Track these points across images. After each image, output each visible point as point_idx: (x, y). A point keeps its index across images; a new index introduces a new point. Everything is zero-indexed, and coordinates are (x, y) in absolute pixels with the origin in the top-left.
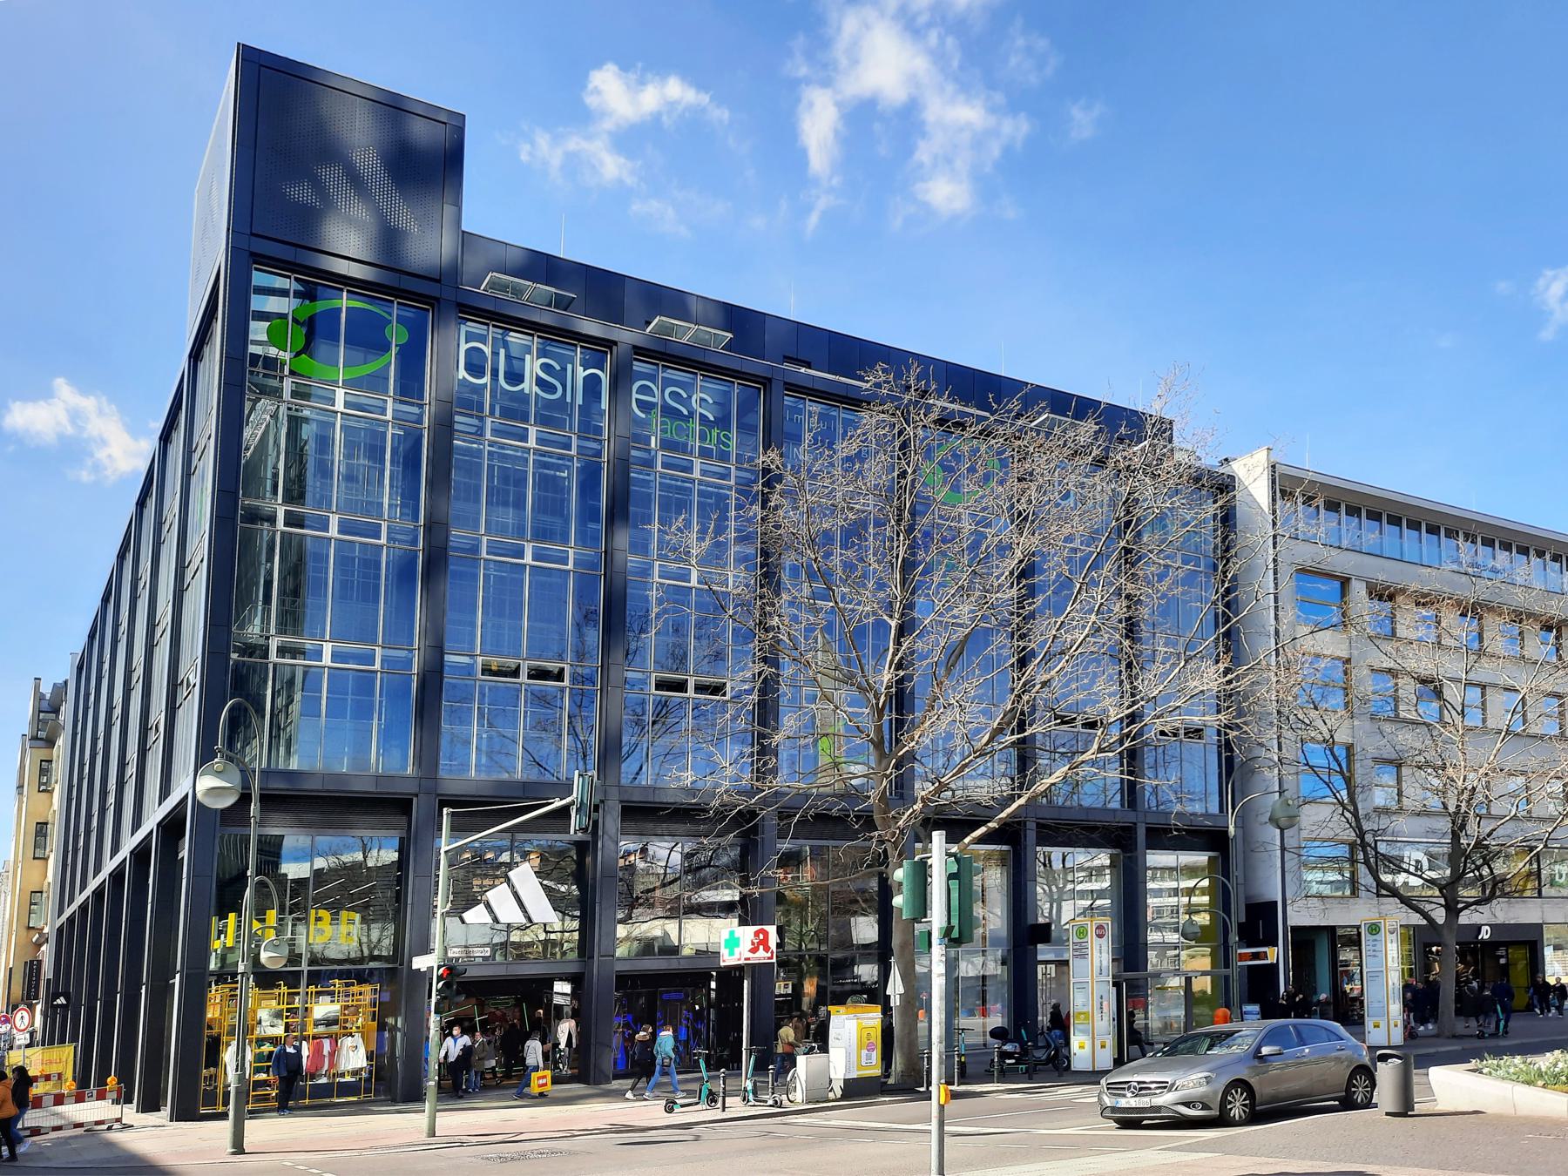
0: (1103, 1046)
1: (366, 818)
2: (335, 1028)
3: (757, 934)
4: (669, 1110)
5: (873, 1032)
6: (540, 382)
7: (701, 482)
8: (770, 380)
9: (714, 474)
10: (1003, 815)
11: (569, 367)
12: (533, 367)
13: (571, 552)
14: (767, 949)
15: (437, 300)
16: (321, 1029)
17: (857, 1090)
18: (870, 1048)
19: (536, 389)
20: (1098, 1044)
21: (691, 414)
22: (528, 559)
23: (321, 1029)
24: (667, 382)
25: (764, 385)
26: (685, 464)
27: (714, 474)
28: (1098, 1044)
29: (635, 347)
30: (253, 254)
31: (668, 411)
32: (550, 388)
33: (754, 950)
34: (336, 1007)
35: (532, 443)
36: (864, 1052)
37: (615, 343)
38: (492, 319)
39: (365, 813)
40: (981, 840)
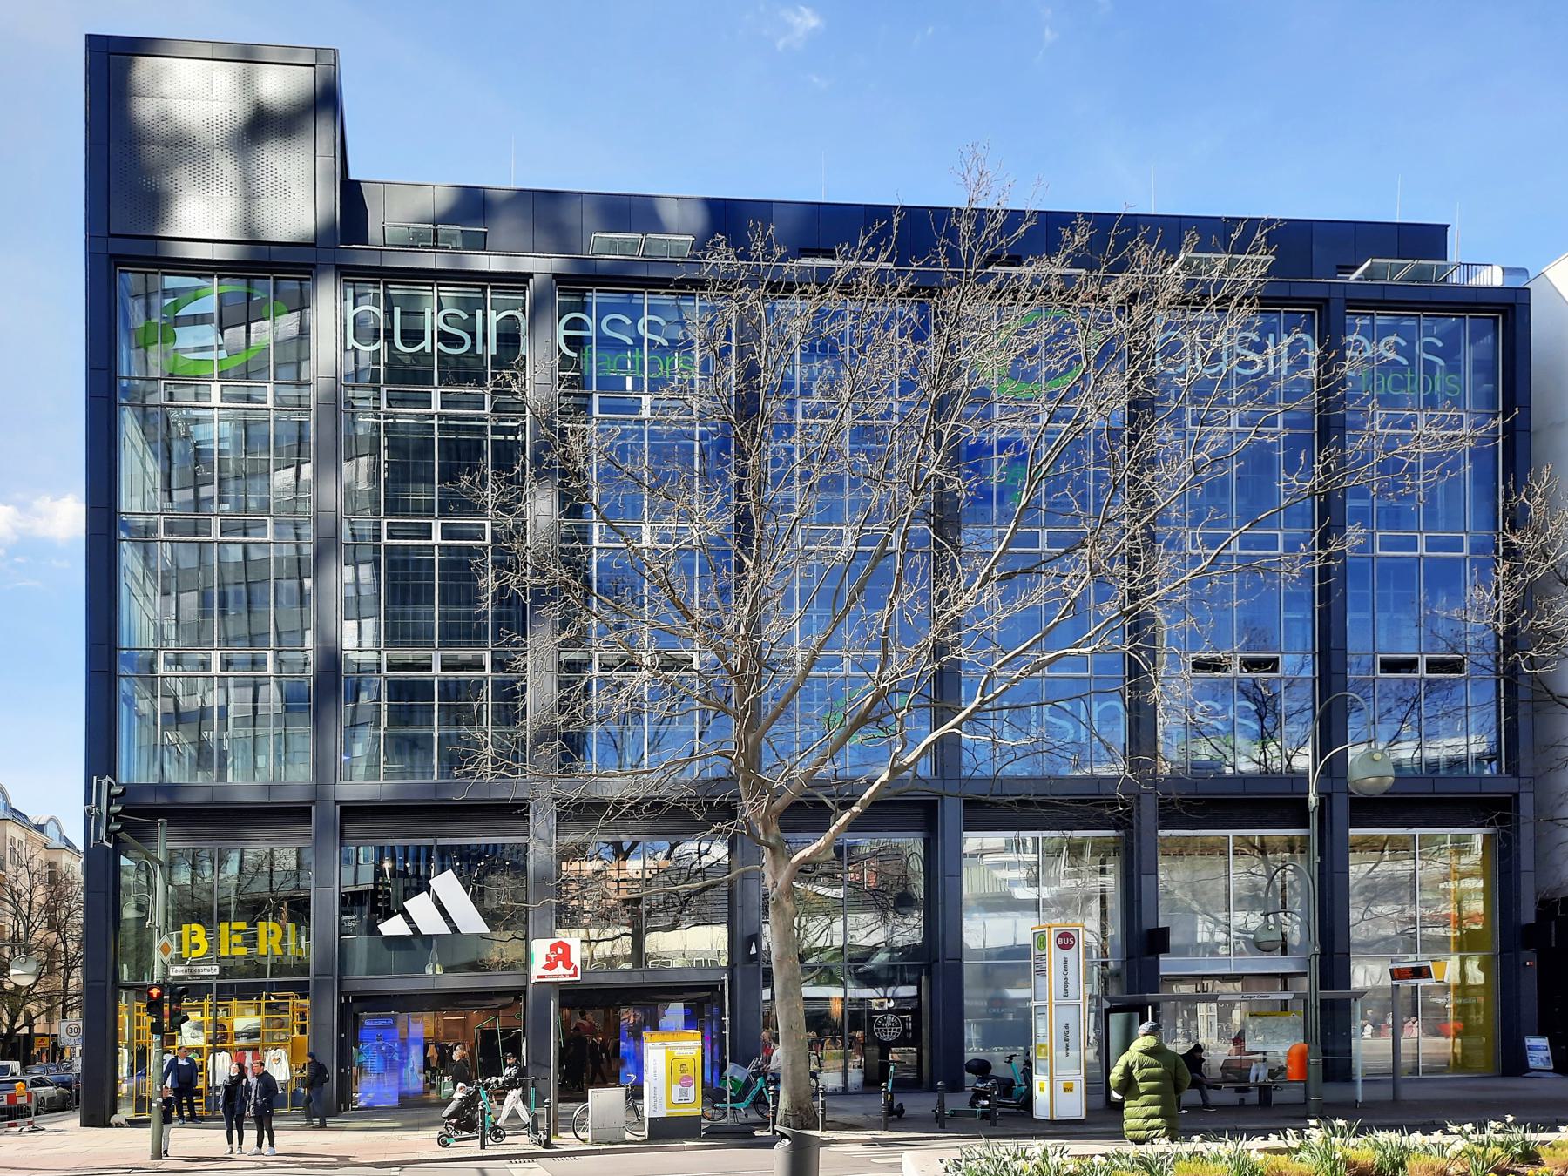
0: (1068, 1089)
1: (208, 830)
2: (257, 1041)
3: (553, 948)
4: (483, 1147)
5: (689, 1064)
6: (444, 337)
7: (441, 417)
8: (1326, 301)
9: (238, 398)
10: (865, 796)
11: (479, 313)
12: (432, 321)
13: (488, 524)
14: (568, 965)
15: (314, 266)
16: (243, 1041)
17: (666, 1131)
18: (686, 1082)
19: (438, 345)
20: (1059, 1086)
21: (639, 340)
22: (436, 538)
23: (243, 1041)
24: (604, 309)
25: (1319, 308)
26: (424, 397)
27: (238, 398)
28: (1059, 1086)
29: (555, 276)
30: (112, 256)
31: (605, 343)
32: (456, 341)
33: (550, 966)
34: (258, 1020)
35: (436, 407)
36: (677, 1087)
37: (531, 275)
38: (647, 287)
39: (472, 820)
40: (855, 826)
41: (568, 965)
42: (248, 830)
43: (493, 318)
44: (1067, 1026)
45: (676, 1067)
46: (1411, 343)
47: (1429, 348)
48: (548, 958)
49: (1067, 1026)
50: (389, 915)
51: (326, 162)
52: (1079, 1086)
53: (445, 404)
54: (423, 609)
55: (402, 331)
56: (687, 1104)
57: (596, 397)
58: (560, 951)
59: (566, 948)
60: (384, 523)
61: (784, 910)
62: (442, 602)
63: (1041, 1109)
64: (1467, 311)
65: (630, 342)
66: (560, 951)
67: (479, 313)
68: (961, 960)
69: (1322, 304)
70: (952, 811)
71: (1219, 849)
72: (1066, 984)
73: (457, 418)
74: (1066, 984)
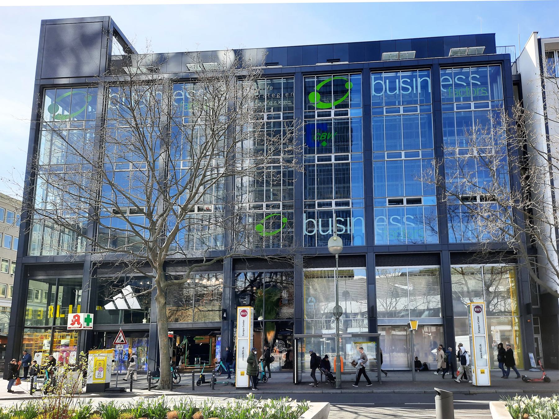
0: (483, 372)
2: (68, 348)
3: (74, 317)
11: (414, 79)
14: (79, 323)
33: (73, 324)
41: (79, 323)
42: (66, 271)
43: (419, 80)
44: (480, 345)
45: (98, 364)
46: (467, 77)
47: (474, 78)
48: (72, 321)
49: (480, 345)
50: (107, 302)
51: (104, 51)
52: (487, 370)
53: (335, 115)
54: (330, 186)
55: (487, 84)
56: (99, 378)
57: (384, 108)
58: (77, 318)
59: (79, 317)
60: (386, 153)
61: (159, 302)
62: (336, 183)
63: (238, 385)
64: (488, 64)
65: (465, 84)
66: (77, 318)
67: (414, 79)
68: (452, 317)
69: (430, 66)
70: (445, 256)
71: (330, 276)
72: (479, 327)
73: (341, 119)
74: (479, 327)
